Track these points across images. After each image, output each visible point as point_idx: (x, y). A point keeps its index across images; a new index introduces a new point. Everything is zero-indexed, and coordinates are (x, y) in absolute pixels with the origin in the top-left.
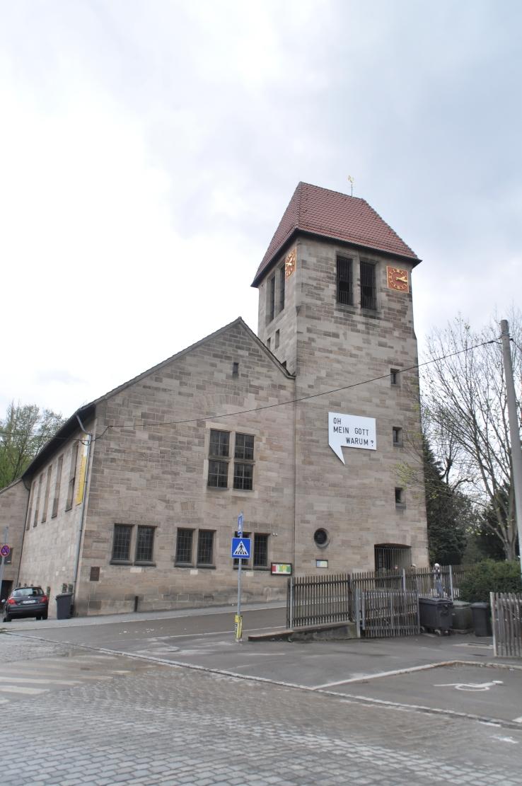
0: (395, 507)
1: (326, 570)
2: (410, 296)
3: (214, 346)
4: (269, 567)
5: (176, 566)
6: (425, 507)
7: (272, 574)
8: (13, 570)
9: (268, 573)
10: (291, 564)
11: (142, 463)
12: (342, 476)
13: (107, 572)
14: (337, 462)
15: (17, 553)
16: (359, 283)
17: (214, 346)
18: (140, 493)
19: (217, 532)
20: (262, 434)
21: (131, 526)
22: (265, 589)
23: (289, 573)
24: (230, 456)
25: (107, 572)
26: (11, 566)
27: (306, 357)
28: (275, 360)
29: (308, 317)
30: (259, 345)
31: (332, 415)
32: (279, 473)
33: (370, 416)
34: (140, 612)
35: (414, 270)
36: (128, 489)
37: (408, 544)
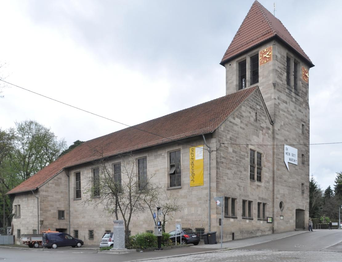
0: (301, 192)
1: (282, 220)
2: (308, 84)
3: (250, 102)
4: (266, 219)
5: (243, 218)
6: (309, 193)
7: (268, 222)
8: (66, 223)
9: (266, 221)
10: (272, 218)
11: (231, 165)
12: (287, 177)
13: (224, 221)
14: (286, 170)
15: (67, 213)
16: (293, 74)
17: (250, 102)
18: (231, 181)
19: (253, 202)
20: (264, 153)
21: (229, 198)
22: (266, 229)
23: (271, 222)
24: (255, 164)
25: (224, 221)
26: (65, 220)
27: (277, 113)
28: (268, 114)
29: (278, 90)
30: (263, 104)
31: (286, 146)
32: (268, 174)
33: (296, 148)
34: (235, 240)
35: (311, 69)
36: (228, 179)
37: (304, 210)
